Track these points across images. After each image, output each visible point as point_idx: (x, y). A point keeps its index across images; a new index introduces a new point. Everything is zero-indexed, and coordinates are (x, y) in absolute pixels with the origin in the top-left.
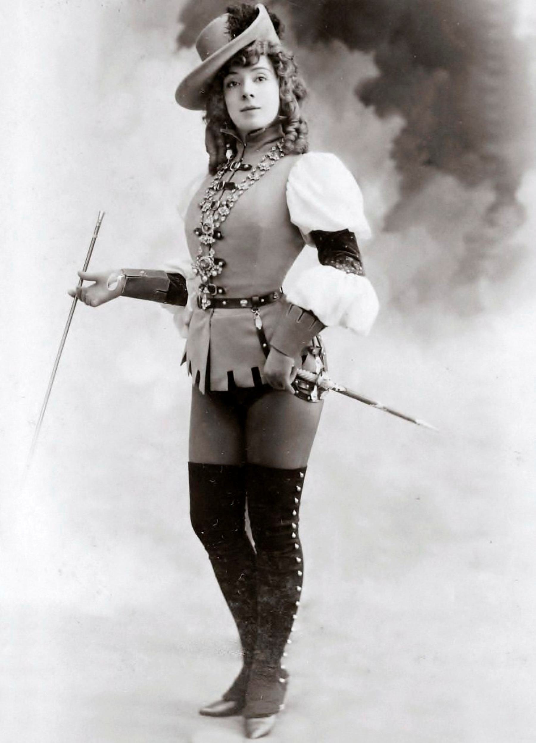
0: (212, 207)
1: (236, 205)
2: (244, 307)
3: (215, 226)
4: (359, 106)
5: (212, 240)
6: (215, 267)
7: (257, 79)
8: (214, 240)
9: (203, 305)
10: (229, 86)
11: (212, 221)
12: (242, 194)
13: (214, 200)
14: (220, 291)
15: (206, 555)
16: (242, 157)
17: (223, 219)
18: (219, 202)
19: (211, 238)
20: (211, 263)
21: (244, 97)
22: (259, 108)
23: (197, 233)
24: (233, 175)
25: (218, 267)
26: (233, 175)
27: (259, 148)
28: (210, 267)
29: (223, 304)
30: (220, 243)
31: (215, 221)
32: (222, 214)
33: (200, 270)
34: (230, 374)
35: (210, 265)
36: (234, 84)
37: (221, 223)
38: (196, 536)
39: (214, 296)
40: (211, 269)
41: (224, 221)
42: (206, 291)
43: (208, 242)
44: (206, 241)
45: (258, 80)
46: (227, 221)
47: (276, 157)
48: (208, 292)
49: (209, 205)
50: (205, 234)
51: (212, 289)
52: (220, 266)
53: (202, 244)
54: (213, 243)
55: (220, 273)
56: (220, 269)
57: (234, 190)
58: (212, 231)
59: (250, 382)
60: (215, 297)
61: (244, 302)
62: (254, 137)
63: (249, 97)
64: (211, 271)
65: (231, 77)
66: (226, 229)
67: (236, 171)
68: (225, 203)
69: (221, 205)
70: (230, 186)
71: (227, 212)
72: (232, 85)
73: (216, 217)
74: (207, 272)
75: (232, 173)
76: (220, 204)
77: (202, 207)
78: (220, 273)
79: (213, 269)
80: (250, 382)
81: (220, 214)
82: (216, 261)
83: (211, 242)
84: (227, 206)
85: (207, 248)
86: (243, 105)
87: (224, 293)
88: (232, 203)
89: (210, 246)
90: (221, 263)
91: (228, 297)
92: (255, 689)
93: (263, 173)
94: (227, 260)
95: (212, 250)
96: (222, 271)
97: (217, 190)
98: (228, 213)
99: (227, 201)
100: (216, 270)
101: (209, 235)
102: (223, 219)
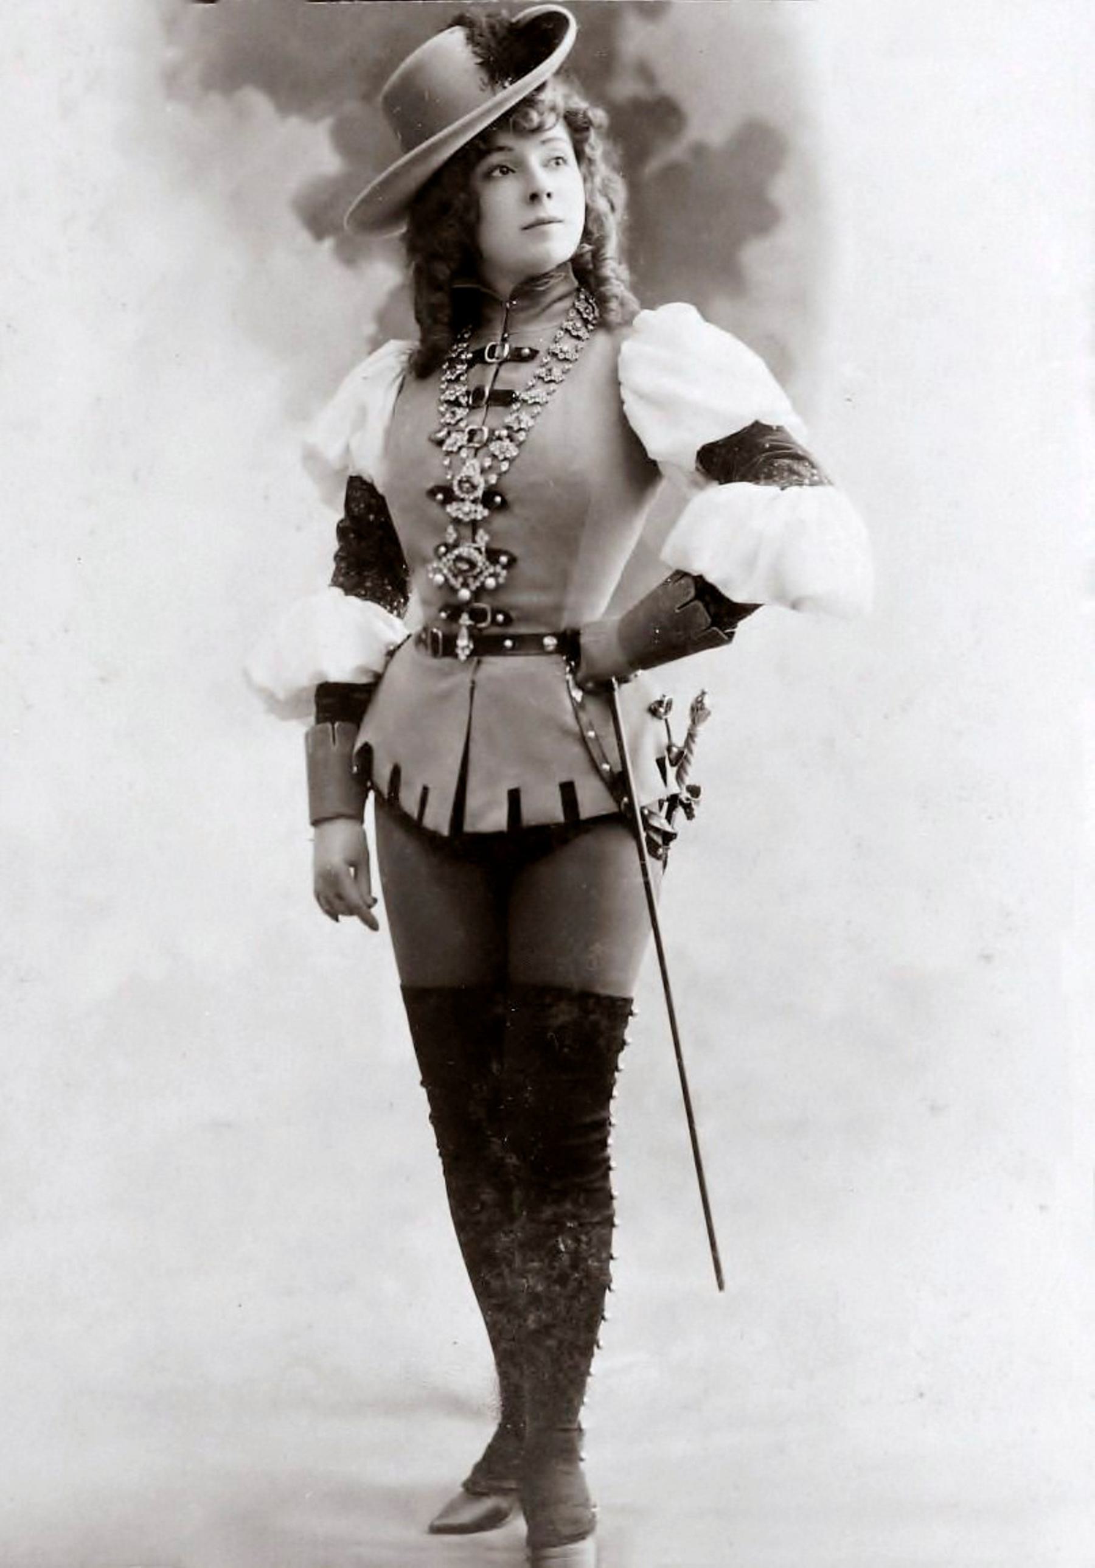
0: (470, 440)
1: (533, 434)
2: (550, 653)
3: (486, 482)
4: (304, 237)
5: (481, 512)
6: (491, 570)
7: (549, 161)
8: (486, 512)
9: (459, 651)
10: (488, 176)
11: (478, 470)
12: (538, 413)
13: (475, 427)
14: (500, 618)
15: (617, 1109)
16: (505, 331)
17: (505, 466)
18: (486, 430)
19: (480, 508)
20: (480, 559)
21: (534, 197)
22: (560, 221)
23: (440, 496)
24: (497, 372)
25: (498, 568)
26: (497, 372)
27: (537, 316)
28: (478, 570)
29: (504, 647)
30: (501, 522)
31: (483, 471)
32: (501, 457)
33: (450, 576)
34: (514, 797)
35: (480, 564)
36: (505, 170)
37: (501, 475)
38: (428, 1135)
39: (480, 630)
40: (481, 572)
41: (505, 472)
42: (465, 620)
43: (472, 516)
44: (467, 514)
45: (553, 163)
46: (513, 470)
47: (582, 333)
48: (469, 623)
49: (462, 438)
50: (463, 500)
51: (477, 615)
52: (504, 567)
53: (457, 521)
54: (484, 518)
55: (501, 580)
56: (504, 573)
57: (519, 405)
58: (479, 493)
59: (558, 814)
60: (485, 632)
61: (550, 642)
62: (531, 286)
63: (545, 197)
64: (482, 578)
65: (496, 158)
66: (514, 486)
67: (500, 364)
68: (505, 433)
69: (493, 437)
70: (505, 398)
71: (513, 451)
72: (497, 173)
73: (488, 462)
74: (470, 580)
75: (494, 368)
76: (492, 432)
77: (440, 443)
78: (501, 580)
79: (486, 573)
80: (558, 814)
81: (494, 457)
82: (492, 555)
83: (479, 517)
84: (510, 437)
85: (467, 532)
86: (530, 217)
87: (508, 620)
88: (523, 433)
89: (474, 525)
90: (504, 559)
91: (511, 630)
92: (531, 1454)
93: (567, 366)
94: (516, 551)
95: (481, 532)
96: (506, 578)
97: (468, 405)
98: (515, 454)
99: (509, 428)
100: (494, 575)
101: (474, 501)
102: (505, 466)
